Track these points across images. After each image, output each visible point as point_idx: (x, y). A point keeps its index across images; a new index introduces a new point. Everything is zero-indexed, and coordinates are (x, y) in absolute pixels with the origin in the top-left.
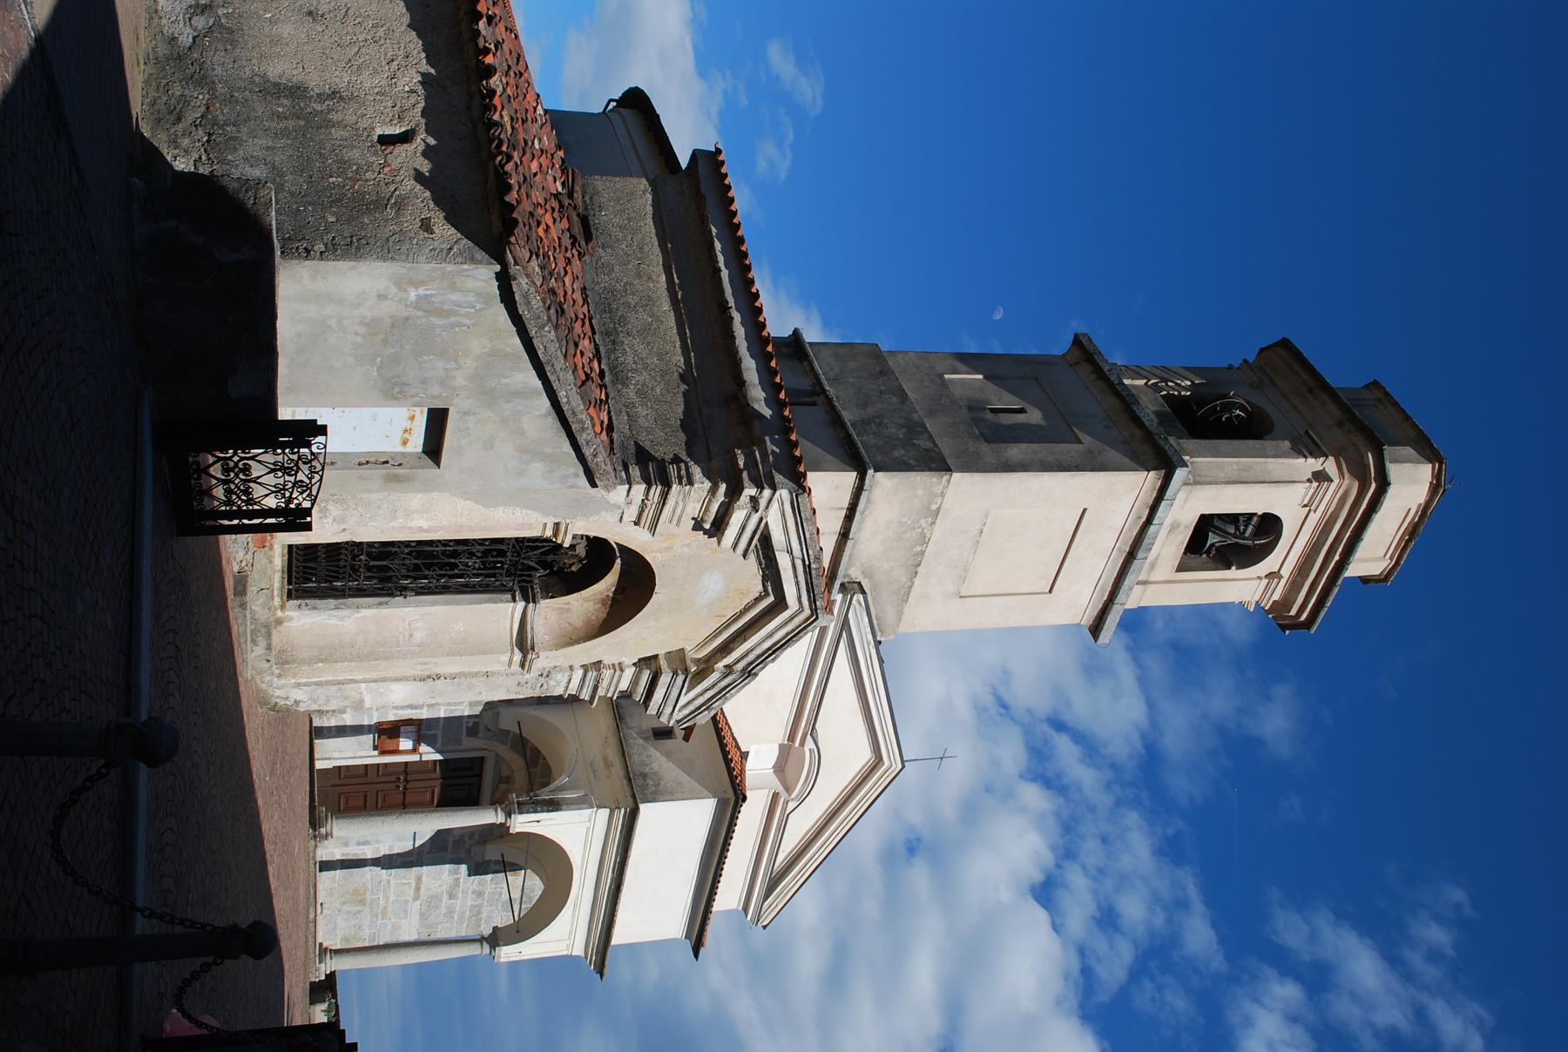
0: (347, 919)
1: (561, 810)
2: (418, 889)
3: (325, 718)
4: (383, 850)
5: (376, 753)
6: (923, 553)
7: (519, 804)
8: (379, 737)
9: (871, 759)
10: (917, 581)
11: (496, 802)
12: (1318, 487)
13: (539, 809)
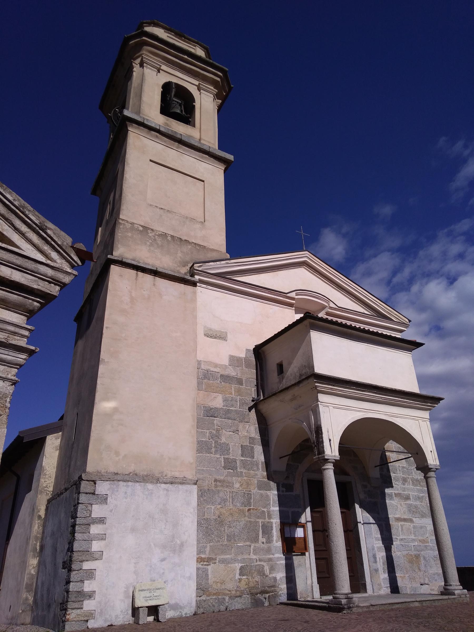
0: (430, 567)
1: (321, 425)
2: (405, 520)
3: (281, 592)
4: (379, 544)
5: (307, 554)
6: (172, 237)
7: (319, 454)
8: (294, 552)
9: (304, 268)
10: (190, 241)
11: (320, 472)
12: (146, 63)
13: (321, 440)
